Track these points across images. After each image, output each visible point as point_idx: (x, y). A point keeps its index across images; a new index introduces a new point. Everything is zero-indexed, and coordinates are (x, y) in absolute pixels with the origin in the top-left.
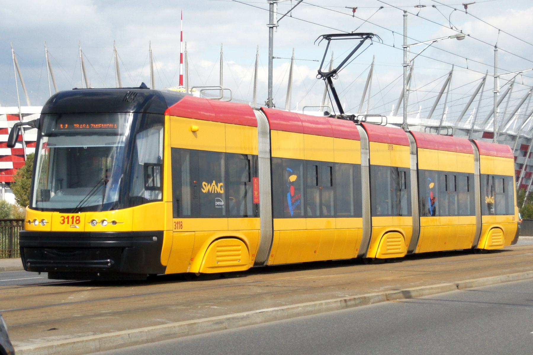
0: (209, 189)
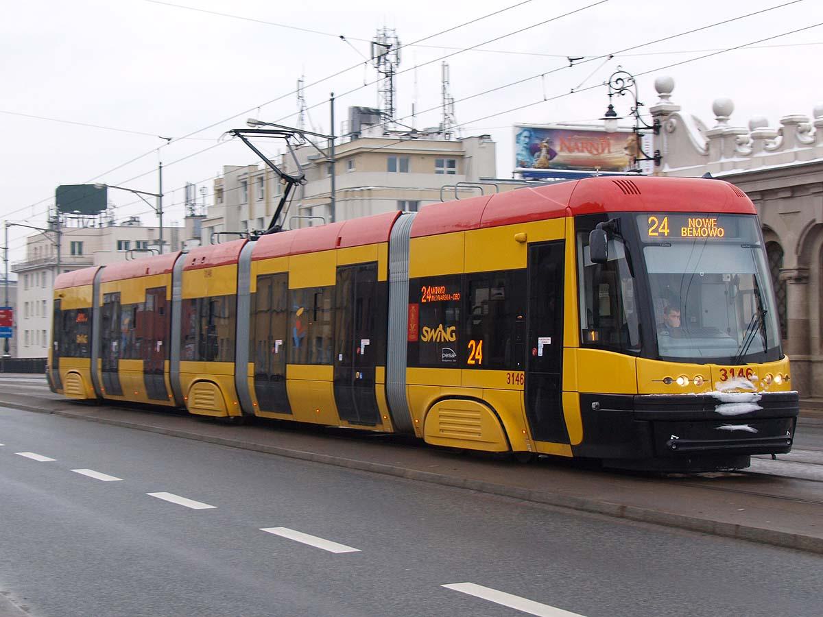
0: (432, 337)
